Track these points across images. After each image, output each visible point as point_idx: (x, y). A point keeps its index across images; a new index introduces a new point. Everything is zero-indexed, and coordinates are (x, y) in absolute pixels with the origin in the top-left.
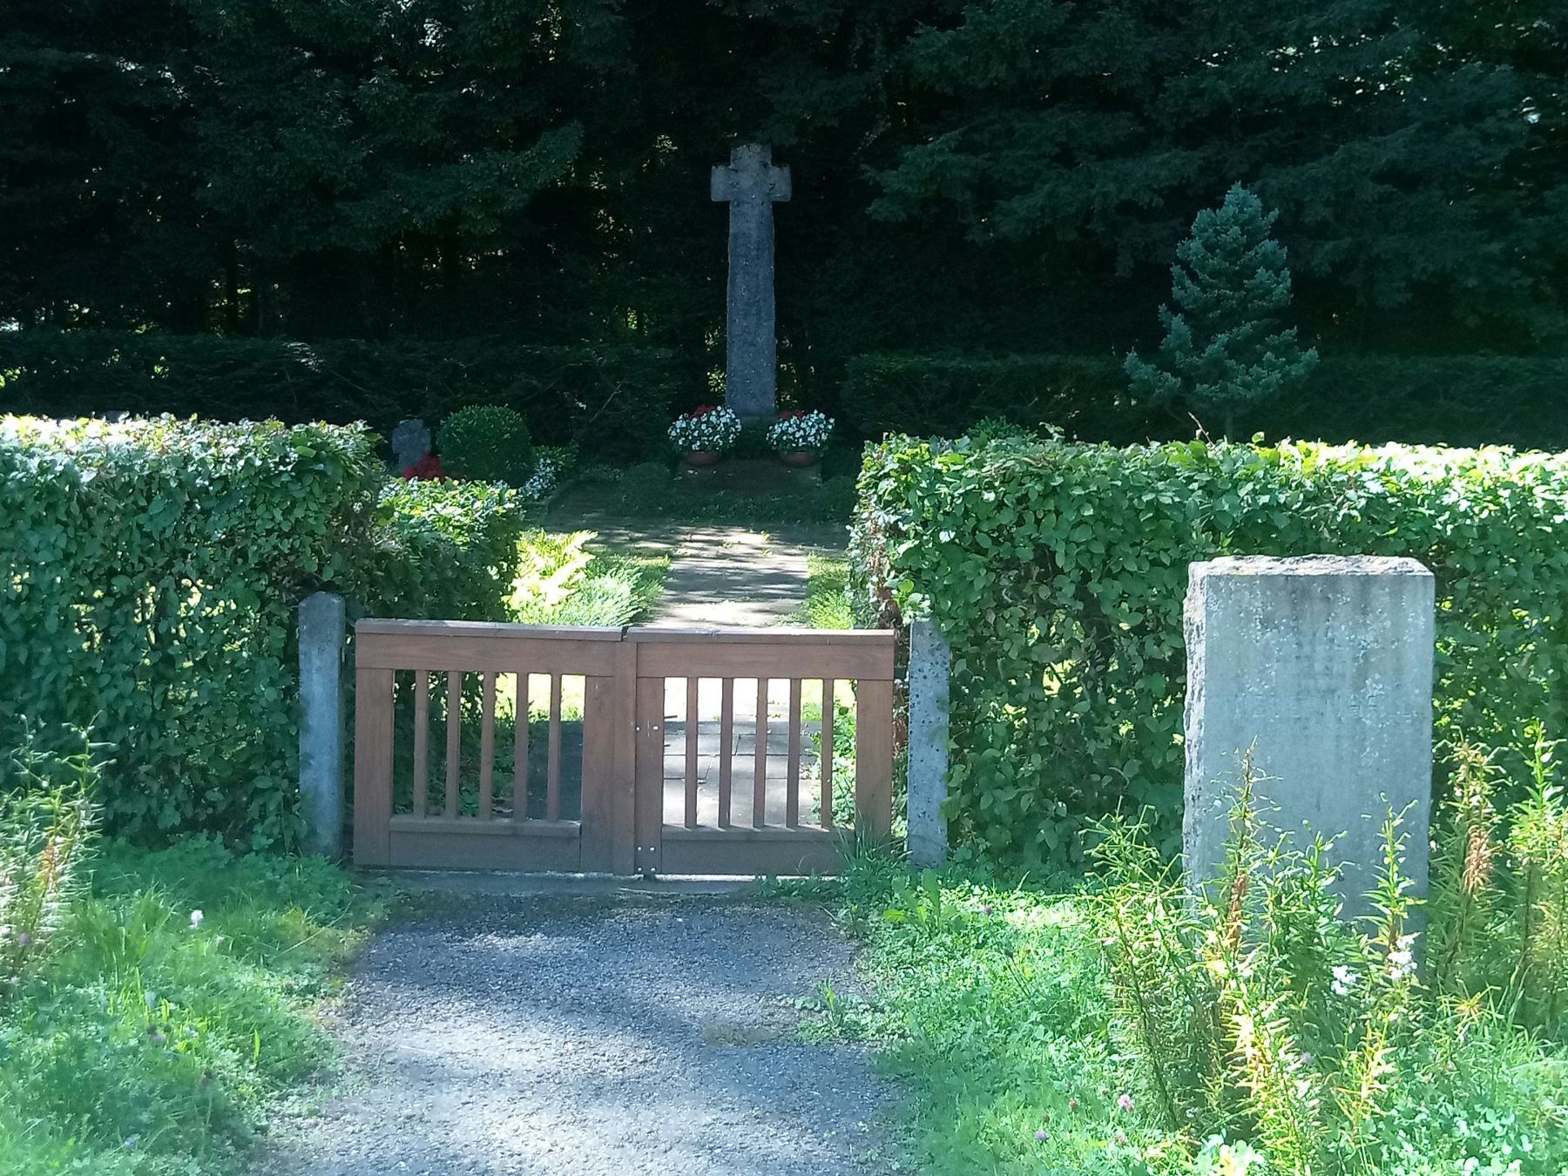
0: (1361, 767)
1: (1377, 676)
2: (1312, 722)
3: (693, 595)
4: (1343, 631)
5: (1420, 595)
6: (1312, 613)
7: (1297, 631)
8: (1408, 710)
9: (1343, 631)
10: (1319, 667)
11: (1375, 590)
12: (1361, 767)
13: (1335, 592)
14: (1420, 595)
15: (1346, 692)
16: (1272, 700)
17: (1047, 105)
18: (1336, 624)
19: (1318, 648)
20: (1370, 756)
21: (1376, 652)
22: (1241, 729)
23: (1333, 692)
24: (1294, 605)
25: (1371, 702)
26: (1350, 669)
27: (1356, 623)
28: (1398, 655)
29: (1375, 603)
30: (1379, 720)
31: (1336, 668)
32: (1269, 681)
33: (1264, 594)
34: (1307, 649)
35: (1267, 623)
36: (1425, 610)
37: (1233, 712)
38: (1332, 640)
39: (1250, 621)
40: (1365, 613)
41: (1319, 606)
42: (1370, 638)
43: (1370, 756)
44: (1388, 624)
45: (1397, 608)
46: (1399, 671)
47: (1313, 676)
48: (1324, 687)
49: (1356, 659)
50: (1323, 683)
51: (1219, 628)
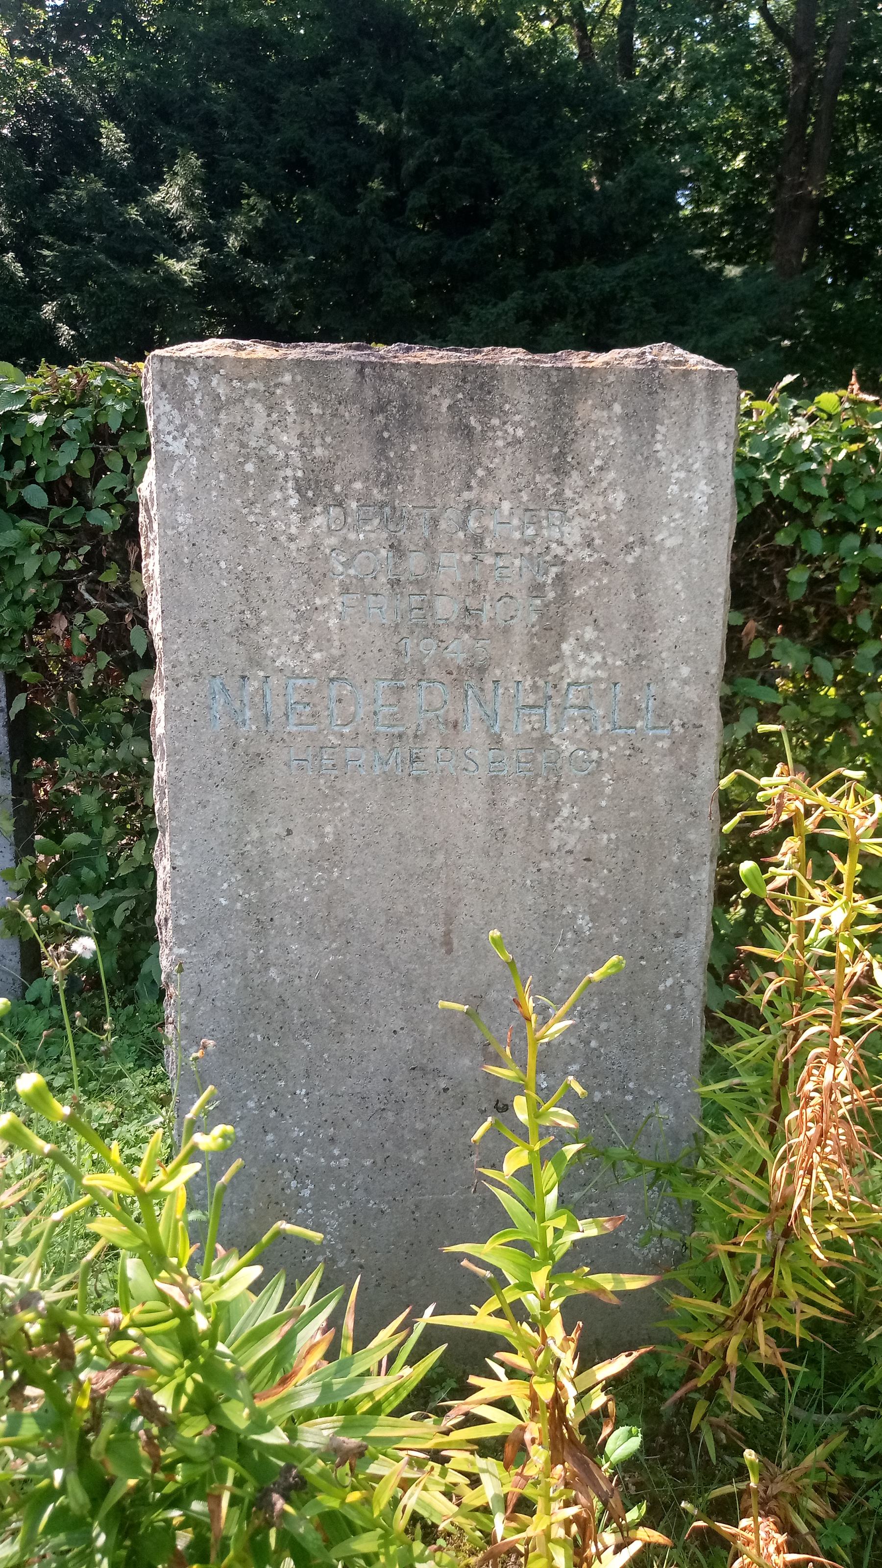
0: (549, 854)
1: (589, 634)
2: (433, 743)
3: (132, 558)
4: (504, 521)
5: (699, 425)
6: (428, 468)
7: (390, 514)
8: (662, 715)
9: (504, 521)
10: (446, 608)
11: (587, 409)
12: (549, 854)
13: (486, 412)
14: (699, 425)
15: (513, 669)
16: (334, 690)
17: (544, 1337)
18: (490, 497)
19: (444, 559)
20: (571, 827)
21: (586, 571)
22: (259, 759)
23: (482, 670)
24: (382, 444)
25: (573, 698)
26: (525, 615)
27: (539, 495)
28: (641, 580)
29: (585, 445)
30: (593, 741)
31: (490, 612)
32: (323, 640)
33: (304, 412)
34: (415, 562)
35: (315, 488)
36: (711, 468)
37: (235, 716)
38: (477, 541)
39: (270, 484)
40: (560, 470)
41: (445, 449)
42: (573, 534)
43: (571, 827)
44: (618, 499)
45: (641, 458)
46: (643, 620)
47: (430, 631)
48: (460, 659)
49: (537, 589)
50: (458, 648)
51: (192, 500)
